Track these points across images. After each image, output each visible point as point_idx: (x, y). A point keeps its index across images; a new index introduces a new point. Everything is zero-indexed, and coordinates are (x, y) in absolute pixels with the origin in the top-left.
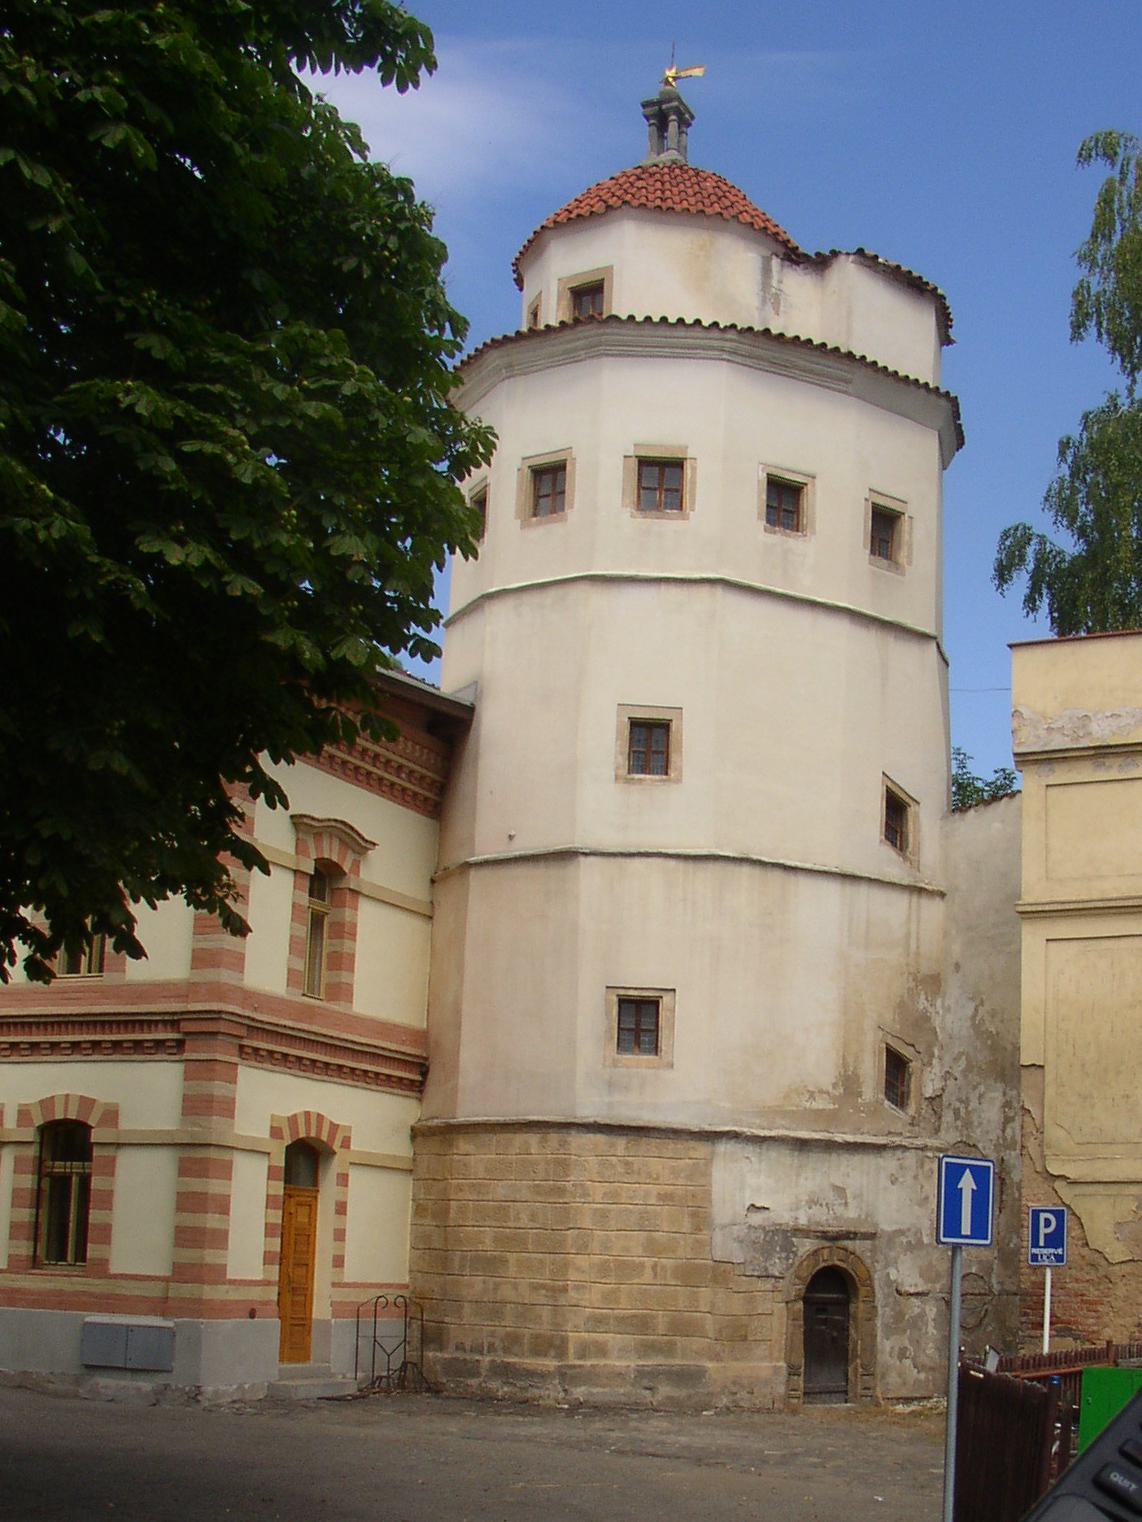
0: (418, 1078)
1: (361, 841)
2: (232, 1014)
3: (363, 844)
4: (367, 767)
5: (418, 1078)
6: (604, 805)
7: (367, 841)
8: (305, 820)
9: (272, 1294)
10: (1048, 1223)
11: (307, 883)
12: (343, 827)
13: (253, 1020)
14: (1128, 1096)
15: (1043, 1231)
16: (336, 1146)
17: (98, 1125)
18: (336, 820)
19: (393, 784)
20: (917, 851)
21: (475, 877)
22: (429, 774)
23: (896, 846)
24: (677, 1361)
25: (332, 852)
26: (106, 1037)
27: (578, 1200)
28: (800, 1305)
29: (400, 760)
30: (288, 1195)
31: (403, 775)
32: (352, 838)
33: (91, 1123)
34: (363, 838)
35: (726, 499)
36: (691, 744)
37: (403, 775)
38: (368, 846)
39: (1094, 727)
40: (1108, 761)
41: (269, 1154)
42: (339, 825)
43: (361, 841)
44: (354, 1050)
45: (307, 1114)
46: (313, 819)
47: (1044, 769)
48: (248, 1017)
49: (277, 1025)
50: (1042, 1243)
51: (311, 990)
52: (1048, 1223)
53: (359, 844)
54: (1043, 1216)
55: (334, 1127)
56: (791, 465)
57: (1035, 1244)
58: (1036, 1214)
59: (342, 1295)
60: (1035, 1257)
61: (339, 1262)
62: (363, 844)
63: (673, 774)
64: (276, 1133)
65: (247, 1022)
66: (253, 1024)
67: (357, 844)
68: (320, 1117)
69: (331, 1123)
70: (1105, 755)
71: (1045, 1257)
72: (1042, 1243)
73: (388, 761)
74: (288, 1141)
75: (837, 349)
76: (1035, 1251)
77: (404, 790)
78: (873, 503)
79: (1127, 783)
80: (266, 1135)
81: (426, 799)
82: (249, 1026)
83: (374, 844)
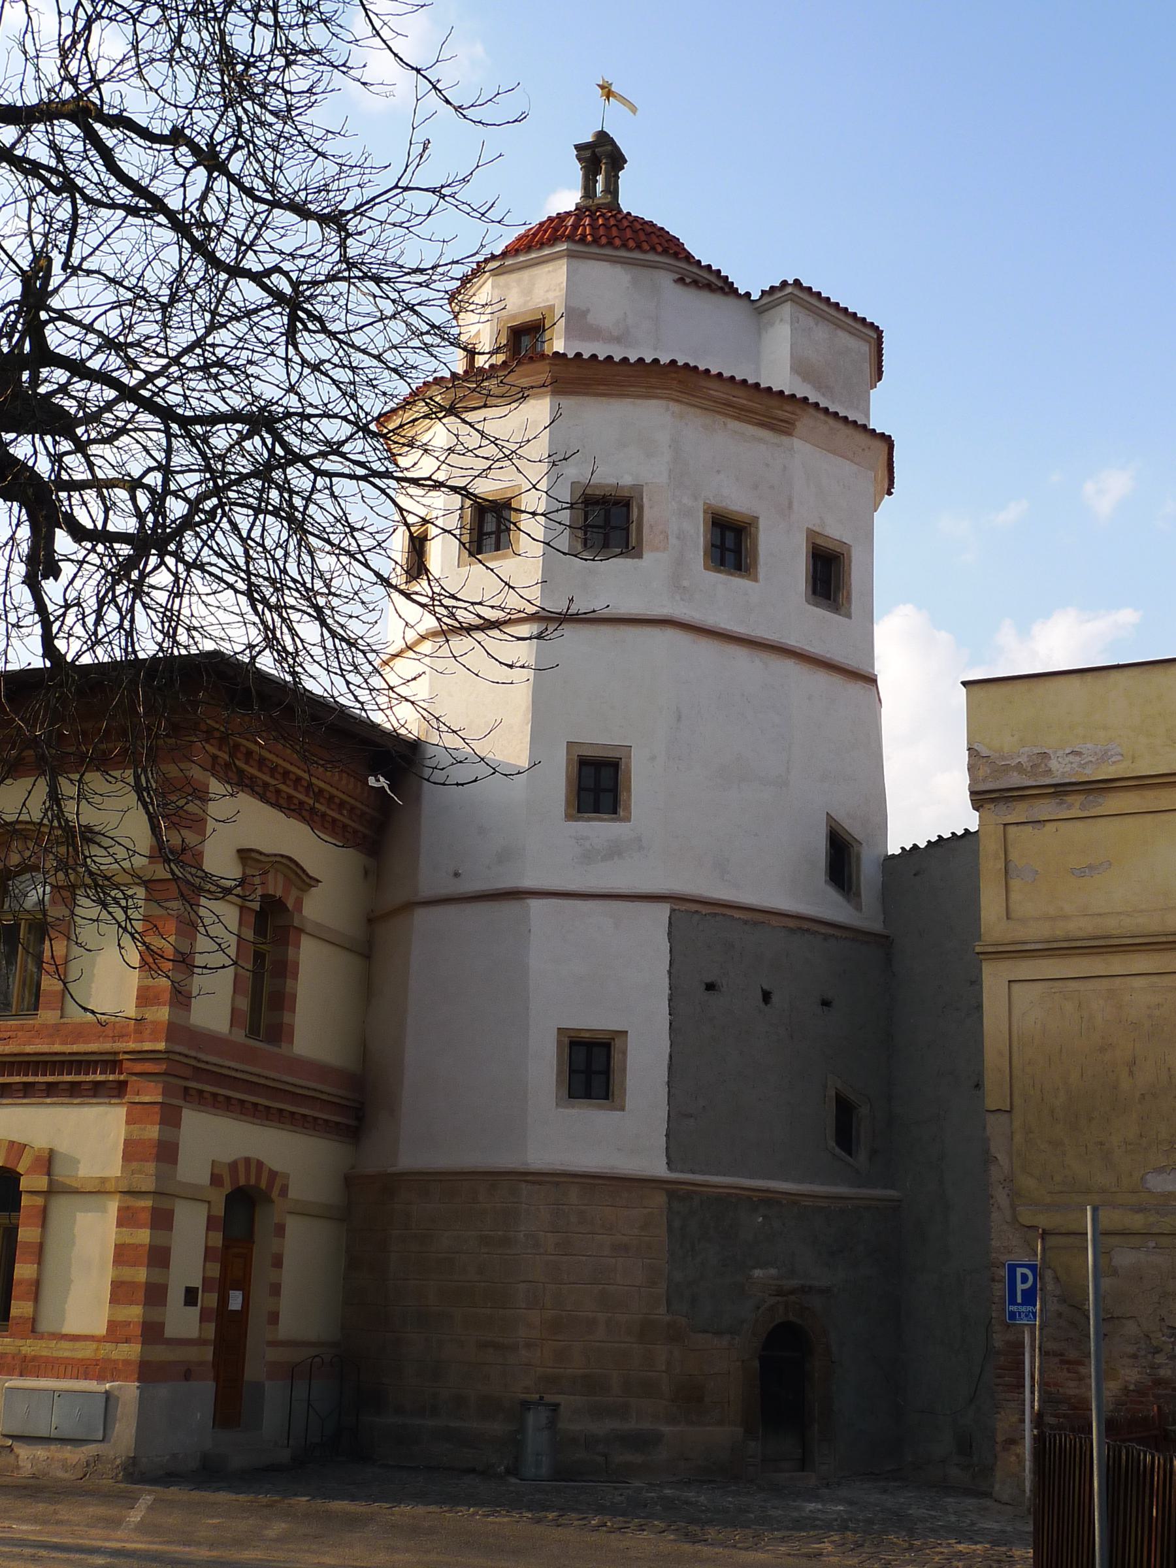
0: (353, 1123)
1: (304, 877)
2: (180, 1054)
3: (307, 880)
4: (311, 802)
5: (353, 1123)
6: (554, 847)
7: (311, 878)
8: (254, 855)
9: (208, 1353)
10: (1025, 1278)
11: (251, 919)
12: (288, 863)
13: (199, 1060)
14: (1101, 1144)
15: (1020, 1287)
16: (275, 1194)
17: (27, 1172)
18: (282, 856)
19: (334, 821)
20: (858, 895)
21: (421, 916)
22: (368, 810)
23: (843, 889)
24: (631, 1425)
25: (275, 886)
26: (17, 1079)
27: (529, 1251)
28: (756, 1363)
29: (344, 797)
30: (226, 1246)
31: (345, 812)
32: (296, 874)
33: (20, 1170)
34: (307, 875)
35: (673, 528)
36: (643, 784)
37: (345, 812)
38: (313, 883)
39: (1054, 764)
40: (1069, 799)
41: (209, 1202)
42: (284, 861)
43: (304, 877)
44: (294, 1093)
45: (247, 1161)
46: (261, 853)
47: (1002, 807)
48: (195, 1058)
49: (222, 1066)
50: (1019, 1300)
51: (253, 1031)
52: (1025, 1278)
53: (304, 881)
54: (1019, 1271)
55: (273, 1175)
56: (737, 502)
57: (1013, 1301)
58: (1012, 1269)
59: (272, 1355)
60: (1013, 1315)
61: (274, 1318)
62: (307, 880)
63: (622, 813)
64: (216, 1180)
65: (193, 1062)
66: (199, 1065)
67: (303, 880)
68: (260, 1164)
69: (270, 1169)
70: (1066, 793)
71: (1023, 1315)
72: (1019, 1300)
73: (332, 797)
74: (227, 1189)
75: (745, 381)
76: (1014, 1308)
77: (345, 826)
78: (811, 534)
79: (1089, 820)
80: (205, 1180)
81: (355, 832)
82: (194, 1067)
83: (318, 881)
